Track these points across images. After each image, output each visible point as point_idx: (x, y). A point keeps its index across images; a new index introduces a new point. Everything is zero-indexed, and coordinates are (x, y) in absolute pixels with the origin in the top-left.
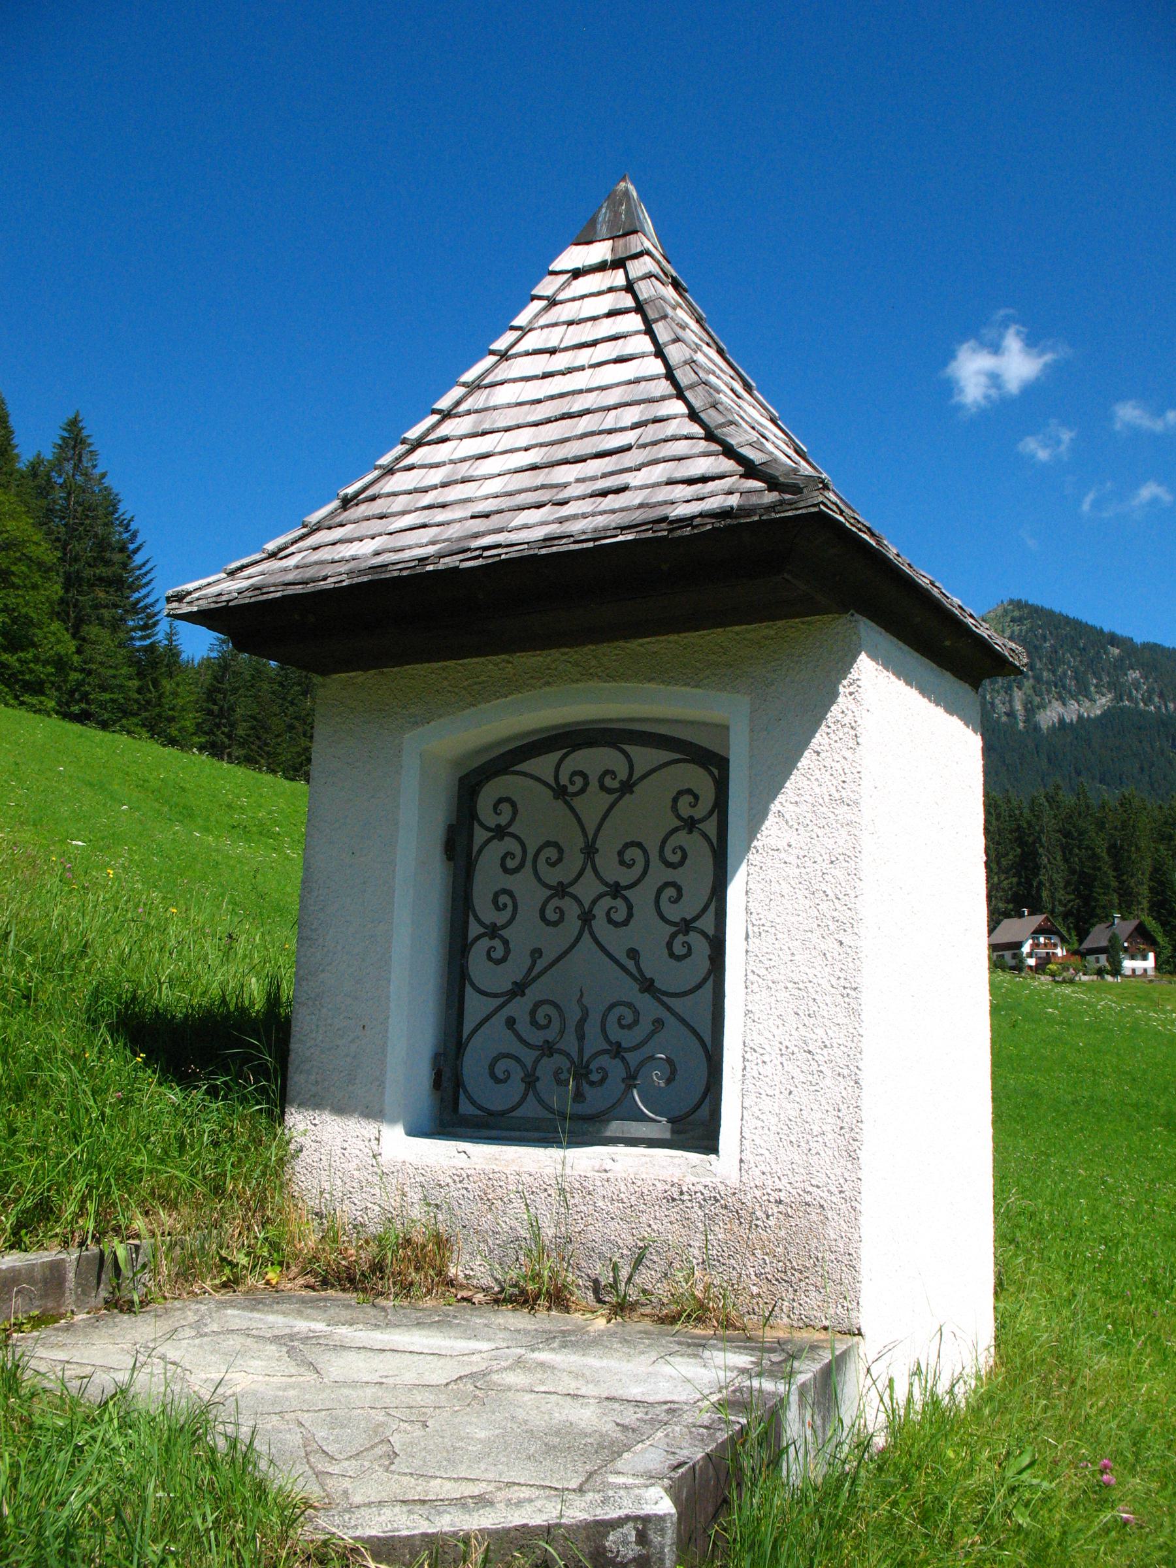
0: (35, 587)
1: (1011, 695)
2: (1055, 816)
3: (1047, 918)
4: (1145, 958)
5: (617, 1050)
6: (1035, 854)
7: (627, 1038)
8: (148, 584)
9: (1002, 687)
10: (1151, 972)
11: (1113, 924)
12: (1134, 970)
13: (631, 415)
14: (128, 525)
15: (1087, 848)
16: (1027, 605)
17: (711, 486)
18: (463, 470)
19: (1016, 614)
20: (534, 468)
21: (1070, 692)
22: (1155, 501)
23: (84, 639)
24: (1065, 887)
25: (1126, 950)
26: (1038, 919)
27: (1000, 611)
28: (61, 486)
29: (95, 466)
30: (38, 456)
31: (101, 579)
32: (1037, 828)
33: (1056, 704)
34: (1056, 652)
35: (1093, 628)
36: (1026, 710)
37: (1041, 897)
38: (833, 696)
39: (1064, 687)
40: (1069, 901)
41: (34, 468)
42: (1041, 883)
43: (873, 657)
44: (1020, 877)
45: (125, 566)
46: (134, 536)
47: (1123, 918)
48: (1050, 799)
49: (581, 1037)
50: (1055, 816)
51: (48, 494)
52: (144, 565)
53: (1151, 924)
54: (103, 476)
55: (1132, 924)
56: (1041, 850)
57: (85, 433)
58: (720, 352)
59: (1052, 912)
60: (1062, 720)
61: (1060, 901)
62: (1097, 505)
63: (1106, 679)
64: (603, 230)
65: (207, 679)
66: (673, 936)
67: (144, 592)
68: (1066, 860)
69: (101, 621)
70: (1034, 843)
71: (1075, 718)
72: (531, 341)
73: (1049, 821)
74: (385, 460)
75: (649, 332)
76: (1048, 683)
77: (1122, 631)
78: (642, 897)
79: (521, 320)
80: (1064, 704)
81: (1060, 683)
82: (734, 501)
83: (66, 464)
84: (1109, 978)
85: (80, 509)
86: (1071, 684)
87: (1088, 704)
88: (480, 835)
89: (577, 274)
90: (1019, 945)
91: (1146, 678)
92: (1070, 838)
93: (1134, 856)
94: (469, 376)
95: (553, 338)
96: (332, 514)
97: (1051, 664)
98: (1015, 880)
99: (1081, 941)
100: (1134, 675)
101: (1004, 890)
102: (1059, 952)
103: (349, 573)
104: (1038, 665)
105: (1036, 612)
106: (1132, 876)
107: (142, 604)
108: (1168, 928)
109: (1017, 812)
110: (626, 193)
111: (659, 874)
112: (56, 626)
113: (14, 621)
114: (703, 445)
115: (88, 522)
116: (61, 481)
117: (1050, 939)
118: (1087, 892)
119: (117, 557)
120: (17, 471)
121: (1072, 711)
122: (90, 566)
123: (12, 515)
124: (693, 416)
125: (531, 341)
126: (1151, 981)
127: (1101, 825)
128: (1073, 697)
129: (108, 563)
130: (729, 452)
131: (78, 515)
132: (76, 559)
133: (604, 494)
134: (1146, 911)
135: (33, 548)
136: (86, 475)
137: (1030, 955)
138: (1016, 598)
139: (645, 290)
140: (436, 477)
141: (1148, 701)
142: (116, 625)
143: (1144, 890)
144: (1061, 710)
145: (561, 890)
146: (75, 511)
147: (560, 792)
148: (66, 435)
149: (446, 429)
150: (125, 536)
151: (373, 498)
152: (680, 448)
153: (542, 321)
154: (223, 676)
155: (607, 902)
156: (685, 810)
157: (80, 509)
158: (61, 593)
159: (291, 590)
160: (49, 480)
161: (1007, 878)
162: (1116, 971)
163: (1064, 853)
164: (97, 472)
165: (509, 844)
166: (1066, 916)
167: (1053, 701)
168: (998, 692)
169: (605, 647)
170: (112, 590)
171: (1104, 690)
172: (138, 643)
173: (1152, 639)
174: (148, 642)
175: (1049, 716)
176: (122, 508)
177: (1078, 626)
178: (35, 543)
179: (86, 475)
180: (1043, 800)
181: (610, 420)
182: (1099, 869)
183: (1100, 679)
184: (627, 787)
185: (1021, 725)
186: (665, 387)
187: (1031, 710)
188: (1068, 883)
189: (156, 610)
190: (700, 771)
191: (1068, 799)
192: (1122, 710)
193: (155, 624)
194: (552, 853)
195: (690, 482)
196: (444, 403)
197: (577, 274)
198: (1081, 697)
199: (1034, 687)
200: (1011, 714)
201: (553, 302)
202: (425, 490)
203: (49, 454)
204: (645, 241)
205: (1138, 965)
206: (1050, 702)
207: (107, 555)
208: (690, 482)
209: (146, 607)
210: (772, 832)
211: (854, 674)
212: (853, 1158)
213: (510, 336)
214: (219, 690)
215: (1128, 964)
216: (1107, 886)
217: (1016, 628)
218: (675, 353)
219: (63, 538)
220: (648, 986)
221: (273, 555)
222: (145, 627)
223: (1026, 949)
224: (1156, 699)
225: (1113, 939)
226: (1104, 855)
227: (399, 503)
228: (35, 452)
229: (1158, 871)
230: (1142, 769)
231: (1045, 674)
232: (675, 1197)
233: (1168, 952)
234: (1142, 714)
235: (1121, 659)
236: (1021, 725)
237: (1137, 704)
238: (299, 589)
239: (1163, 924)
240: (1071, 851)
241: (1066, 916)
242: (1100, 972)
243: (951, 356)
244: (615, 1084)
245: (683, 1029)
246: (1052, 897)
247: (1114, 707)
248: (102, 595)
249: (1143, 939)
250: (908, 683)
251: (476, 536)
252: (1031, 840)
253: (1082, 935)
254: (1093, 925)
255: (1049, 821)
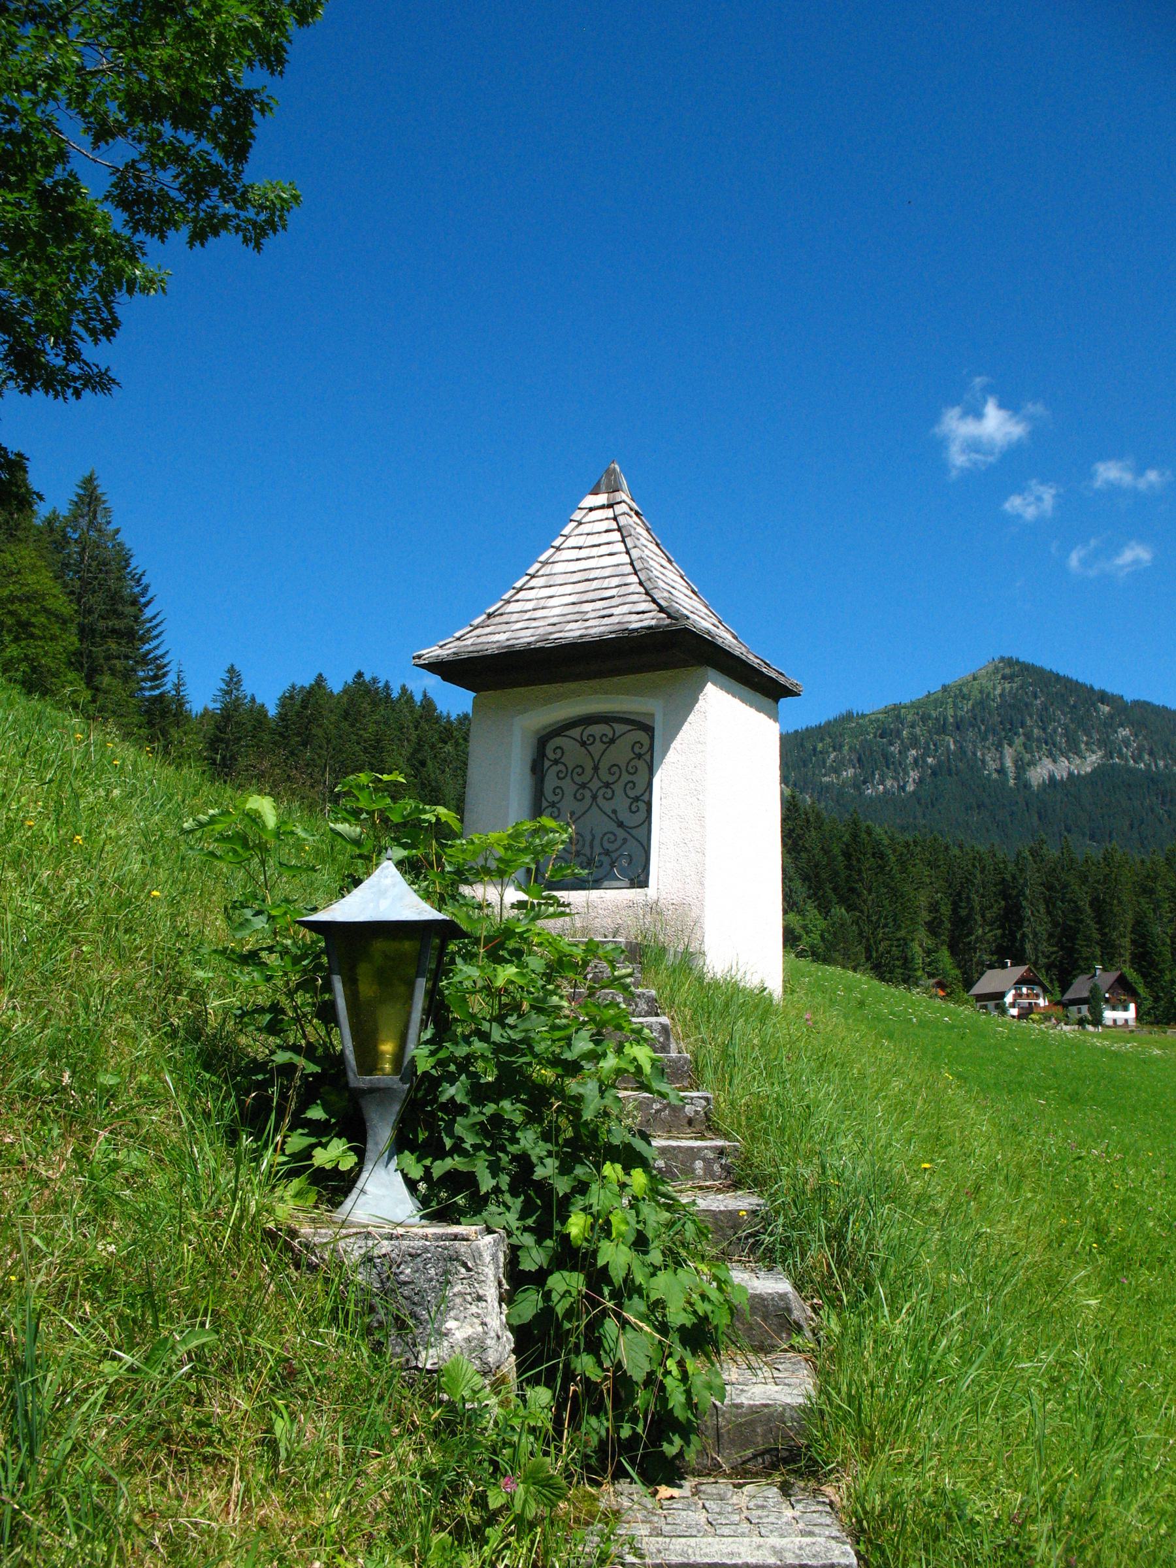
0: (53, 638)
1: (1001, 753)
2: (1038, 871)
3: (1029, 969)
4: (1126, 1009)
5: (607, 853)
6: (1019, 907)
7: (611, 847)
8: (157, 637)
9: (993, 744)
10: (1132, 1023)
11: (1094, 975)
12: (1115, 1021)
13: (615, 581)
14: (139, 579)
15: (1071, 901)
16: (1017, 662)
17: (646, 615)
18: (542, 603)
19: (1007, 671)
20: (574, 604)
21: (1060, 750)
22: (1136, 562)
23: (97, 689)
24: (1048, 940)
25: (1107, 1001)
26: (1021, 970)
27: (991, 669)
28: (76, 541)
29: (109, 523)
30: (54, 512)
31: (114, 631)
32: (1021, 881)
33: (1047, 761)
34: (1047, 709)
35: (1083, 686)
36: (1016, 767)
37: (1024, 950)
38: (696, 700)
39: (1054, 745)
40: (1052, 953)
41: (49, 522)
42: (1024, 935)
43: (715, 684)
44: (1004, 929)
45: (136, 618)
46: (146, 589)
47: (1105, 970)
48: (1033, 852)
49: (592, 847)
50: (1038, 871)
51: (63, 548)
52: (154, 617)
53: (1132, 975)
54: (117, 531)
55: (1113, 976)
56: (1024, 903)
57: (99, 491)
58: (657, 545)
59: (1035, 964)
60: (1052, 777)
61: (1043, 952)
62: (1085, 563)
63: (1096, 736)
64: (603, 488)
65: (209, 728)
66: (631, 804)
67: (154, 643)
68: (1049, 913)
69: (113, 672)
70: (1017, 896)
71: (1065, 775)
72: (571, 542)
73: (1033, 876)
74: (506, 597)
75: (623, 541)
76: (1038, 740)
77: (1112, 689)
78: (618, 788)
79: (565, 531)
80: (1055, 761)
81: (1049, 741)
82: (653, 622)
83: (81, 520)
84: (1090, 1028)
85: (94, 563)
86: (1062, 741)
87: (1078, 761)
88: (547, 763)
89: (591, 509)
90: (1002, 995)
91: (1136, 736)
92: (1053, 892)
93: (1116, 909)
94: (542, 558)
95: (580, 541)
96: (483, 621)
97: (1042, 721)
98: (999, 932)
99: (1063, 992)
100: (1124, 732)
101: (988, 942)
102: (1042, 1002)
103: (498, 648)
104: (1029, 723)
105: (1026, 669)
106: (1114, 929)
107: (151, 656)
108: (1149, 979)
109: (1002, 866)
110: (614, 469)
111: (625, 777)
112: (71, 676)
113: (34, 670)
114: (644, 597)
115: (100, 576)
116: (76, 536)
117: (1032, 989)
118: (1069, 945)
119: (129, 610)
120: (35, 526)
121: (1062, 768)
122: (103, 618)
123: (33, 569)
124: (641, 584)
125: (571, 542)
126: (1132, 1031)
127: (1084, 879)
128: (1062, 754)
129: (120, 615)
130: (654, 601)
131: (92, 569)
132: (90, 611)
133: (603, 617)
134: (1128, 964)
135: (52, 600)
136: (100, 531)
137: (1013, 1005)
138: (1007, 655)
139: (623, 520)
140: (530, 606)
141: (1137, 758)
142: (127, 675)
143: (1126, 942)
144: (1051, 766)
145: (583, 786)
146: (90, 565)
147: (583, 744)
148: (82, 492)
149: (534, 583)
150: (136, 590)
151: (501, 614)
152: (635, 598)
153: (576, 532)
154: (226, 726)
155: (604, 790)
156: (637, 750)
157: (94, 563)
158: (77, 644)
159: (471, 655)
160: (64, 536)
161: (991, 931)
162: (1097, 1021)
163: (1048, 907)
164: (111, 527)
165: (560, 767)
166: (1048, 968)
167: (1044, 758)
168: (989, 749)
169: (603, 680)
170: (123, 641)
171: (1095, 748)
172: (147, 693)
173: (1136, 697)
174: (157, 692)
175: (1039, 774)
176: (134, 563)
177: (1071, 686)
178: (55, 596)
179: (100, 531)
180: (1027, 853)
181: (606, 583)
182: (1082, 921)
183: (1089, 736)
184: (612, 741)
185: (1012, 782)
186: (629, 569)
187: (1021, 767)
188: (1051, 935)
189: (165, 661)
190: (643, 733)
191: (1052, 853)
192: (1113, 766)
193: (165, 675)
194: (579, 770)
195: (638, 613)
196: (531, 571)
197: (591, 509)
198: (1071, 755)
199: (1024, 744)
200: (1001, 771)
201: (580, 523)
202: (526, 612)
203: (64, 510)
204: (623, 496)
205: (1120, 1015)
206: (1040, 759)
207: (120, 608)
208: (638, 613)
209: (157, 658)
210: (671, 756)
211: (705, 691)
212: (702, 884)
213: (561, 539)
214: (221, 740)
215: (1109, 1015)
216: (1088, 939)
217: (1007, 686)
218: (635, 553)
219: (78, 591)
220: (621, 825)
221: (458, 639)
222: (155, 678)
223: (1009, 999)
224: (1146, 757)
225: (1094, 990)
226: (1087, 907)
227: (514, 617)
228: (51, 509)
229: (1139, 924)
230: (1131, 826)
231: (1036, 731)
232: (631, 905)
233: (1148, 1004)
234: (1130, 771)
235: (1111, 716)
236: (1012, 782)
237: (1127, 761)
238: (475, 654)
239: (1144, 976)
240: (1054, 905)
241: (1048, 968)
242: (1081, 1022)
243: (935, 418)
244: (606, 866)
245: (635, 843)
246: (1036, 949)
247: (1104, 765)
248: (114, 646)
249: (1124, 990)
250: (734, 696)
251: (551, 633)
252: (1014, 893)
253: (1065, 987)
254: (1075, 977)
255: (1033, 876)
